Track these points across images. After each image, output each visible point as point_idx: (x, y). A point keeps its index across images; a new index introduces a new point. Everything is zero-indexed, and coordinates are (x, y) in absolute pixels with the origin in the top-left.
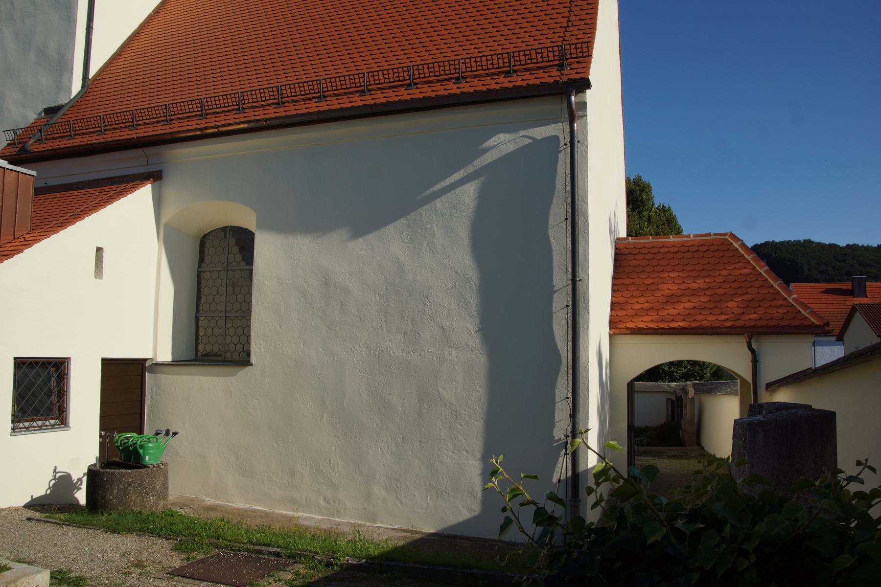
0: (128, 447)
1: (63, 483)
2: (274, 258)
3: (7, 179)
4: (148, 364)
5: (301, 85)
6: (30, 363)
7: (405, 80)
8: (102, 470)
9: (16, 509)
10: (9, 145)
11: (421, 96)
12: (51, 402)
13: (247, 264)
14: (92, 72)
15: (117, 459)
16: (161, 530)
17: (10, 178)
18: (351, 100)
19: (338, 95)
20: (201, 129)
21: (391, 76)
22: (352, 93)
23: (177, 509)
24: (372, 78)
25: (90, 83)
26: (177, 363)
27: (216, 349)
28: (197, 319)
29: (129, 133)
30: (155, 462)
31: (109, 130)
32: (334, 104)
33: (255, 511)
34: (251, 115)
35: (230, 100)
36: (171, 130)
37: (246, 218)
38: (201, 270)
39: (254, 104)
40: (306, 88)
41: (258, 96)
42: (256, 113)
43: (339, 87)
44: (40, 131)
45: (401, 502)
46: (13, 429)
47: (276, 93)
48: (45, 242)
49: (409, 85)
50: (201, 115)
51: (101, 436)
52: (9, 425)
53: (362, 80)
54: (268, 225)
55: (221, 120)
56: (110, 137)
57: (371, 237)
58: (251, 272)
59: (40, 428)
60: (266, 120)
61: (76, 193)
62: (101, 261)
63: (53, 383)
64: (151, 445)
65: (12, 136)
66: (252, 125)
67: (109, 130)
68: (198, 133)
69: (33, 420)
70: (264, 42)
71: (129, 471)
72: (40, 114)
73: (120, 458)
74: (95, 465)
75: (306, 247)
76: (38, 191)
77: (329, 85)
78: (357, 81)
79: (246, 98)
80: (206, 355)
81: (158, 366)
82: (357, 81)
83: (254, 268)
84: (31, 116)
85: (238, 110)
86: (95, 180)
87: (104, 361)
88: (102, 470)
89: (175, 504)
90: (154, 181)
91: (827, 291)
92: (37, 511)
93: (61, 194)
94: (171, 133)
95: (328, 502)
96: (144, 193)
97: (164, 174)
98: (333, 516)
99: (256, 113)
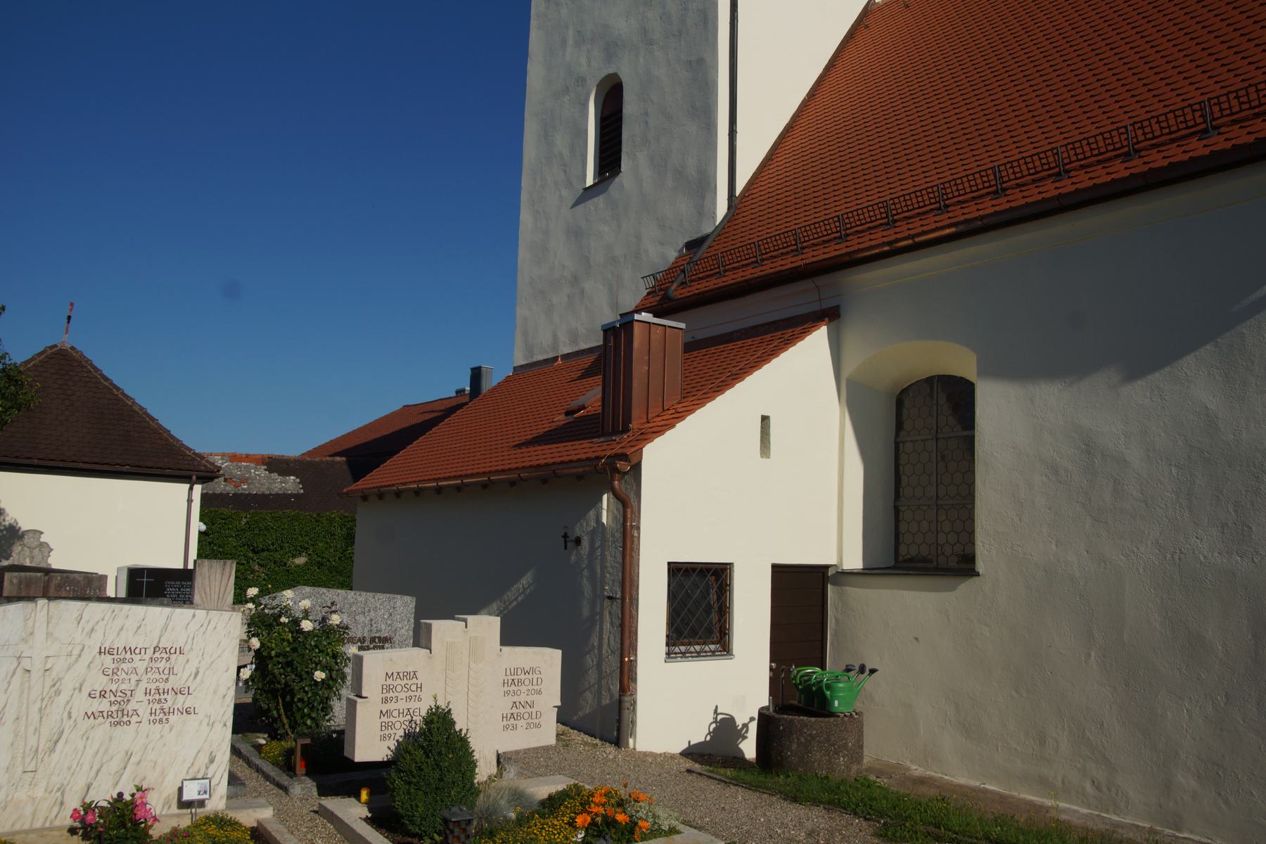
0: (809, 686)
1: (726, 729)
2: (1005, 417)
3: (653, 336)
5: (971, 178)
6: (686, 570)
7: (1196, 125)
8: (777, 716)
9: (672, 757)
10: (649, 294)
11: (1229, 145)
14: (739, 188)
15: (795, 702)
16: (857, 805)
17: (657, 334)
18: (1108, 170)
19: (1089, 166)
20: (889, 243)
22: (1109, 159)
23: (872, 777)
24: (1139, 132)
26: (870, 571)
28: (897, 511)
29: (794, 259)
30: (846, 710)
33: (986, 791)
34: (959, 214)
36: (849, 250)
37: (959, 361)
40: (1037, 163)
42: (965, 211)
43: (1025, 173)
44: (683, 271)
45: (1227, 802)
46: (668, 654)
47: (992, 177)
48: (700, 413)
49: (1205, 131)
50: (888, 224)
51: (771, 669)
52: (663, 649)
54: (993, 369)
56: (768, 268)
57: (1156, 377)
58: (970, 441)
59: (698, 655)
60: (982, 218)
61: (731, 346)
62: (768, 434)
63: (713, 597)
64: (841, 685)
65: (651, 282)
66: (961, 228)
68: (886, 248)
69: (690, 644)
70: (965, 108)
71: (813, 719)
73: (799, 699)
74: (767, 708)
75: (1051, 396)
76: (690, 347)
79: (949, 190)
80: (911, 560)
81: (844, 576)
83: (977, 434)
84: (672, 255)
85: (939, 209)
86: (753, 328)
87: (774, 567)
88: (777, 716)
89: (870, 770)
91: (583, 407)
92: (696, 761)
93: (713, 349)
94: (849, 254)
95: (1098, 789)
96: (819, 339)
97: (842, 311)
98: (1107, 811)
99: (965, 211)
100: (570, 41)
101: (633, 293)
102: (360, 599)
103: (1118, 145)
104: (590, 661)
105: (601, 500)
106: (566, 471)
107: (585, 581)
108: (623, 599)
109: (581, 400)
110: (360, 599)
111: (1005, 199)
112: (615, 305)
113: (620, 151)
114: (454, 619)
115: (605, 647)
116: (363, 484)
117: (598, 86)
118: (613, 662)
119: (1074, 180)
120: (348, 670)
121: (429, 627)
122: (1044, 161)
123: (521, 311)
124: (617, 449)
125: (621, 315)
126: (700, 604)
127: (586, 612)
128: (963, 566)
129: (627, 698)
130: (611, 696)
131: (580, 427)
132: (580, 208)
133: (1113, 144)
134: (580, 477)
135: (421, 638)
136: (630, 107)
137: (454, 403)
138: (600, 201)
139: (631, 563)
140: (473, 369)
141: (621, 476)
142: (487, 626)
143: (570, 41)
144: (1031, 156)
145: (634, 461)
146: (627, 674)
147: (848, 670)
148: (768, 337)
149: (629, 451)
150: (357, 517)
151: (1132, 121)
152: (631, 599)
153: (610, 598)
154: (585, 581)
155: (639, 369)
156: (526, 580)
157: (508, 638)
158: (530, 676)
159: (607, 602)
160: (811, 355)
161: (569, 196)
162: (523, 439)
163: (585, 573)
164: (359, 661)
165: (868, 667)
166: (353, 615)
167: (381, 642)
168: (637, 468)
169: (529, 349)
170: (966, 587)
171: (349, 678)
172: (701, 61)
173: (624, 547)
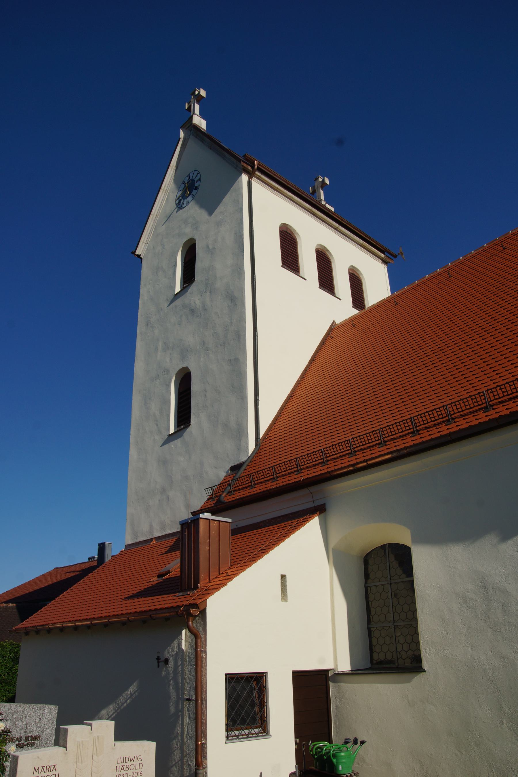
0: (322, 756)
4: (331, 674)
10: (209, 499)
12: (255, 712)
13: (407, 577)
15: (313, 768)
18: (477, 417)
20: (353, 465)
21: (508, 389)
22: (476, 411)
24: (491, 395)
25: (261, 442)
26: (356, 672)
27: (389, 657)
28: (370, 631)
30: (347, 772)
31: (280, 477)
32: (462, 424)
34: (393, 446)
35: (372, 437)
36: (329, 470)
37: (402, 535)
38: (367, 585)
39: (393, 437)
40: (435, 415)
41: (396, 429)
44: (229, 485)
46: (227, 737)
47: (410, 424)
50: (351, 453)
51: (296, 743)
52: (224, 733)
53: (483, 398)
54: (423, 539)
55: (368, 454)
56: (281, 482)
59: (248, 736)
60: (406, 448)
61: (260, 531)
63: (255, 695)
64: (342, 754)
65: (210, 492)
66: (395, 454)
67: (280, 477)
68: (351, 468)
69: (241, 729)
72: (228, 472)
75: (458, 553)
76: (235, 532)
77: (455, 408)
78: (479, 399)
79: (385, 432)
80: (381, 662)
81: (339, 676)
82: (479, 399)
84: (222, 475)
85: (381, 443)
86: (273, 519)
90: (320, 513)
91: (169, 572)
93: (249, 533)
96: (313, 525)
97: (327, 507)
100: (160, 348)
101: (199, 501)
102: (19, 709)
103: (480, 403)
104: (176, 744)
105: (181, 634)
106: (158, 616)
107: (171, 688)
108: (196, 700)
109: (168, 567)
110: (19, 709)
111: (419, 437)
112: (188, 506)
113: (190, 412)
114: (83, 724)
115: (185, 734)
116: (26, 624)
117: (176, 374)
118: (190, 745)
119: (457, 424)
120: (7, 764)
121: (66, 730)
122: (439, 413)
123: (130, 510)
124: (191, 601)
125: (192, 513)
126: (247, 699)
127: (172, 710)
128: (414, 665)
129: (200, 771)
130: (190, 769)
131: (167, 586)
132: (166, 446)
133: (477, 402)
134: (167, 619)
135: (60, 740)
136: (196, 387)
137: (87, 566)
138: (178, 443)
139: (201, 676)
140: (99, 544)
141: (192, 617)
142: (105, 728)
143: (160, 348)
144: (432, 411)
145: (202, 608)
146: (200, 753)
147: (346, 742)
148: (283, 524)
149: (198, 602)
150: (21, 644)
151: (486, 389)
152: (202, 701)
153: (188, 700)
154: (171, 688)
155: (203, 549)
156: (132, 689)
157: (121, 735)
158: (134, 763)
159: (186, 703)
160: (309, 535)
161: (160, 440)
162: (131, 593)
163: (172, 683)
164: (15, 759)
165: (359, 740)
166: (14, 721)
167: (31, 741)
168: (203, 612)
169: (135, 534)
170: (418, 679)
171: (8, 769)
172: (237, 360)
173: (196, 665)
